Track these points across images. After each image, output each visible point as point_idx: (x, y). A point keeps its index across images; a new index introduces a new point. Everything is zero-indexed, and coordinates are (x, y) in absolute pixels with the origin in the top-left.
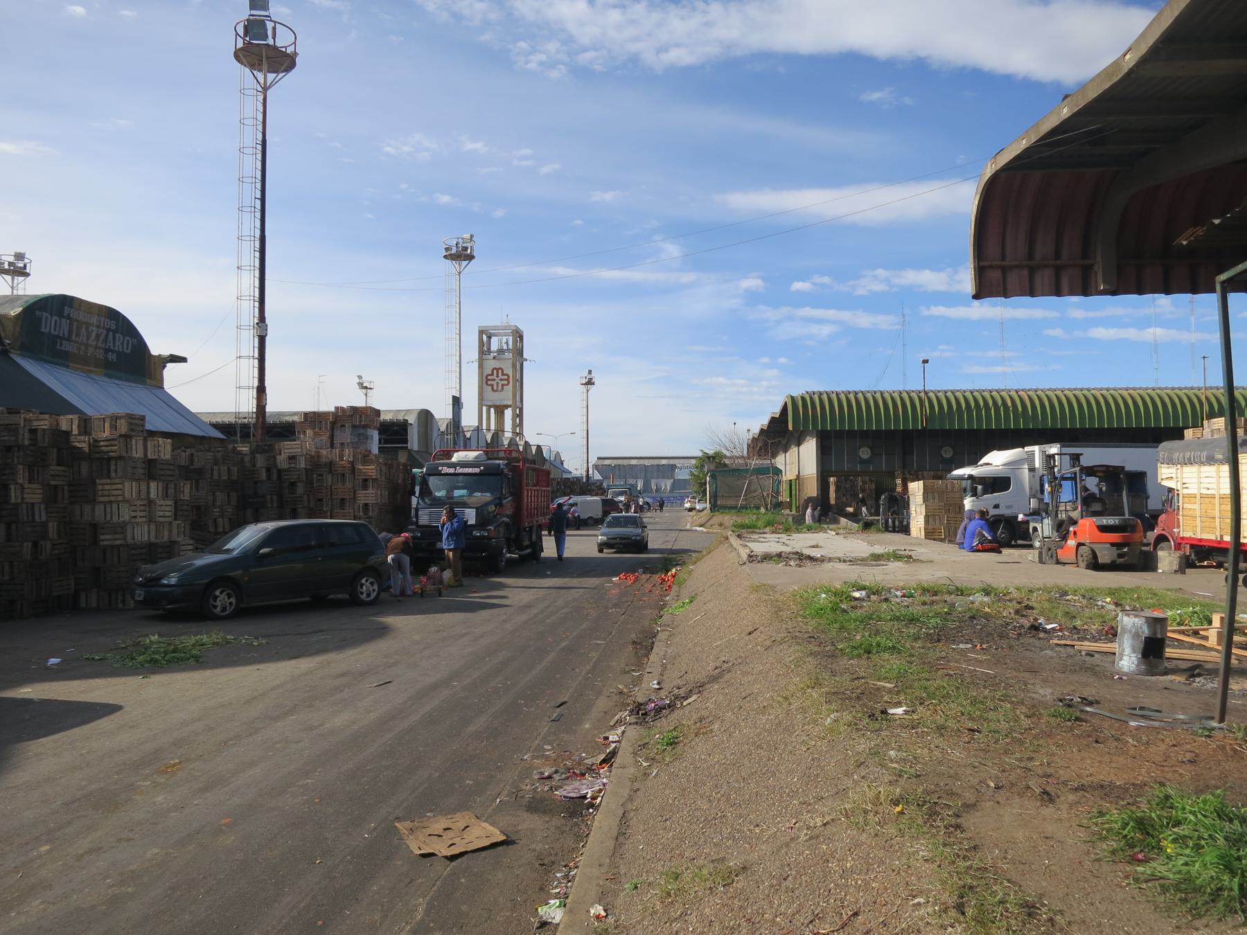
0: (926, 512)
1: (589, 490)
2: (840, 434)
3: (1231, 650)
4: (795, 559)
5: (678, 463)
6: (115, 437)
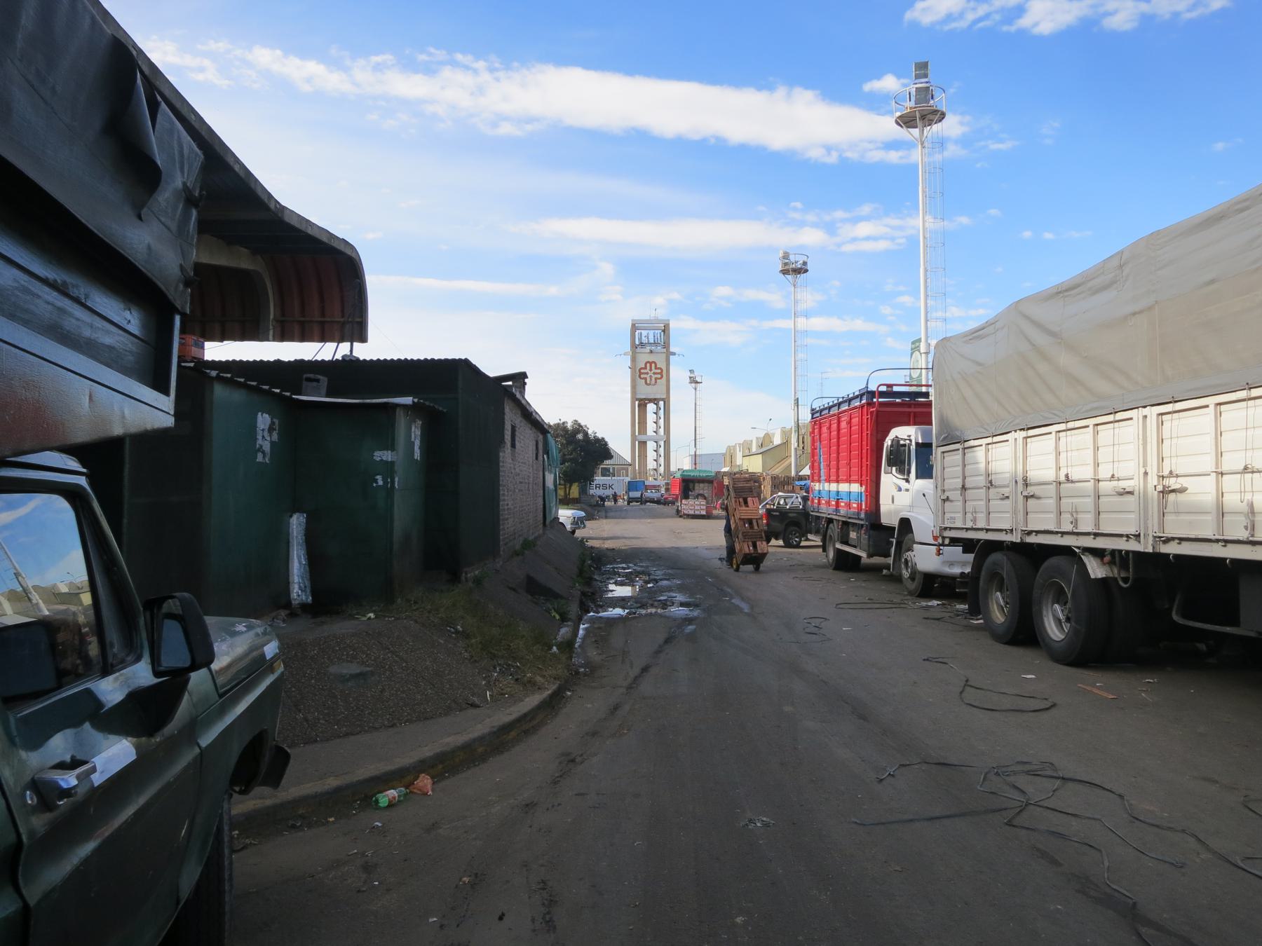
3: (784, 541)
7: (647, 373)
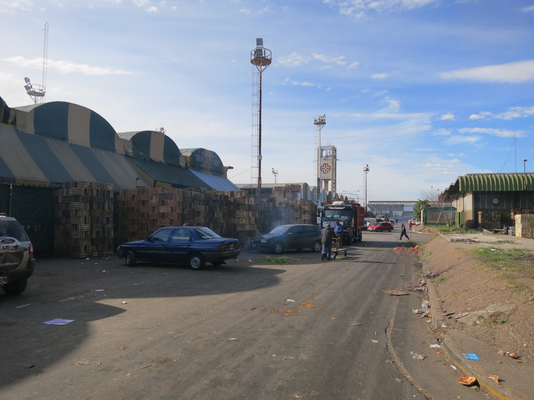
0: (522, 227)
1: (368, 216)
2: (483, 193)
4: (469, 242)
5: (405, 204)
6: (241, 197)
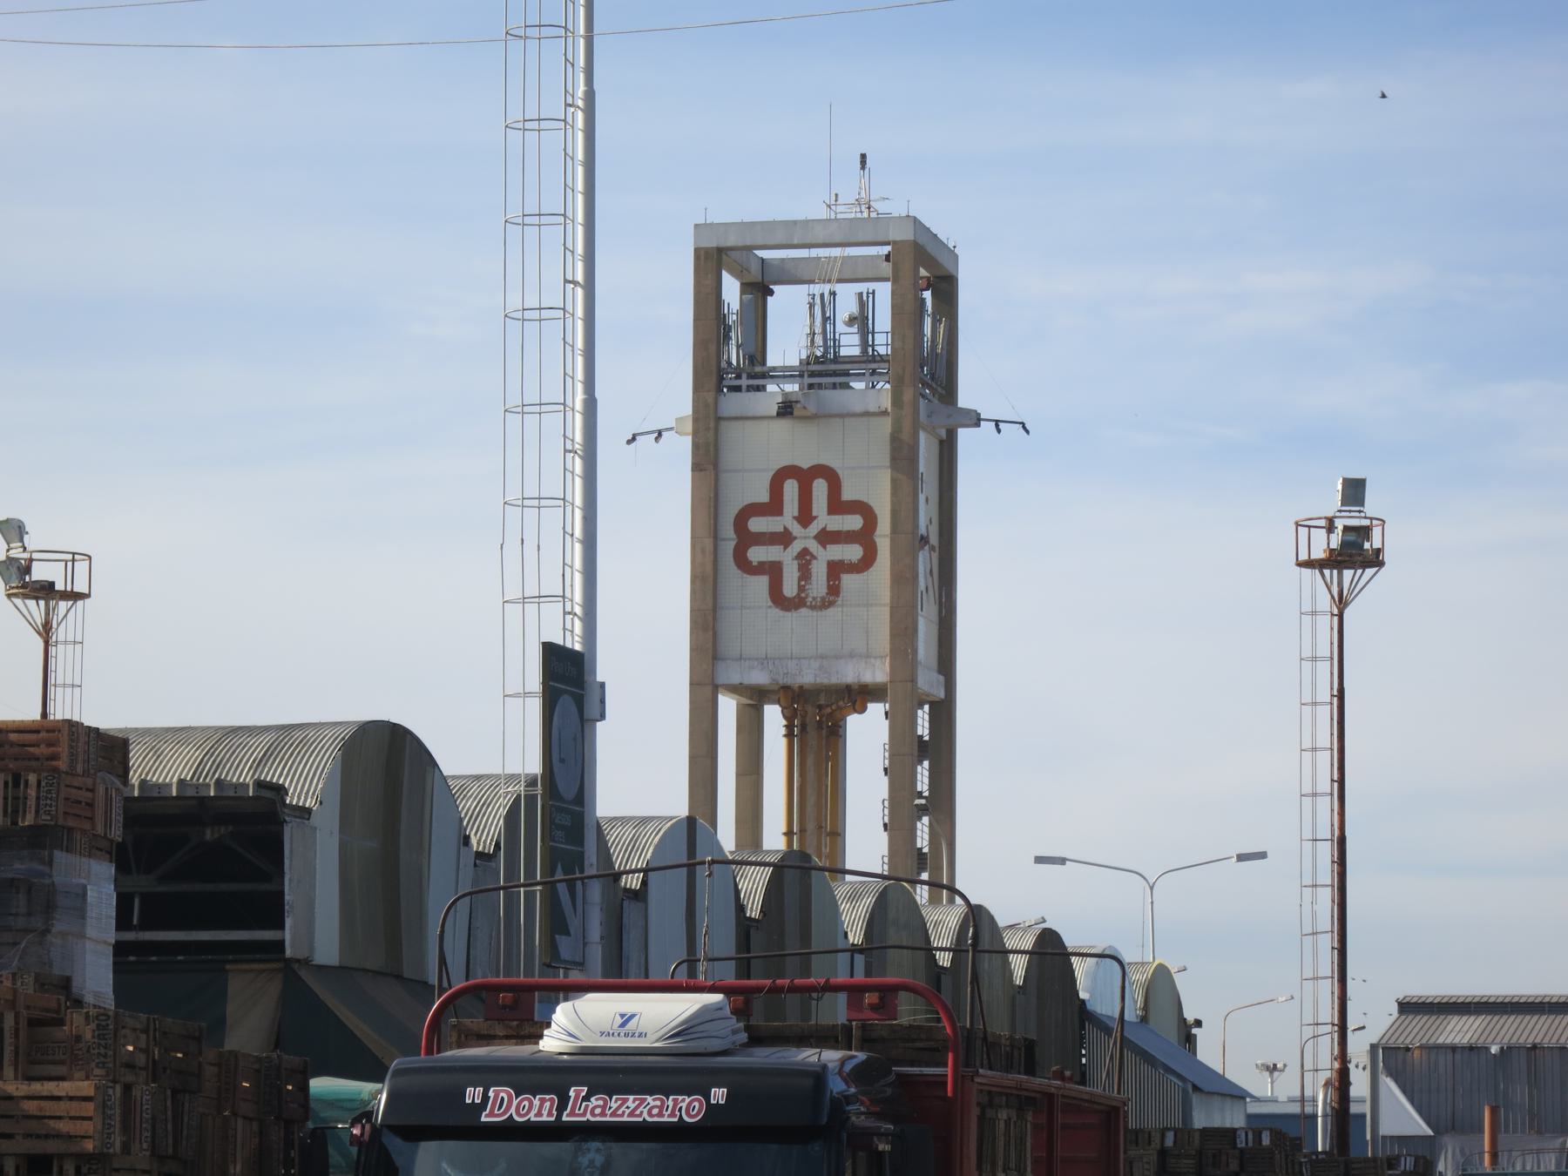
7: (784, 538)
